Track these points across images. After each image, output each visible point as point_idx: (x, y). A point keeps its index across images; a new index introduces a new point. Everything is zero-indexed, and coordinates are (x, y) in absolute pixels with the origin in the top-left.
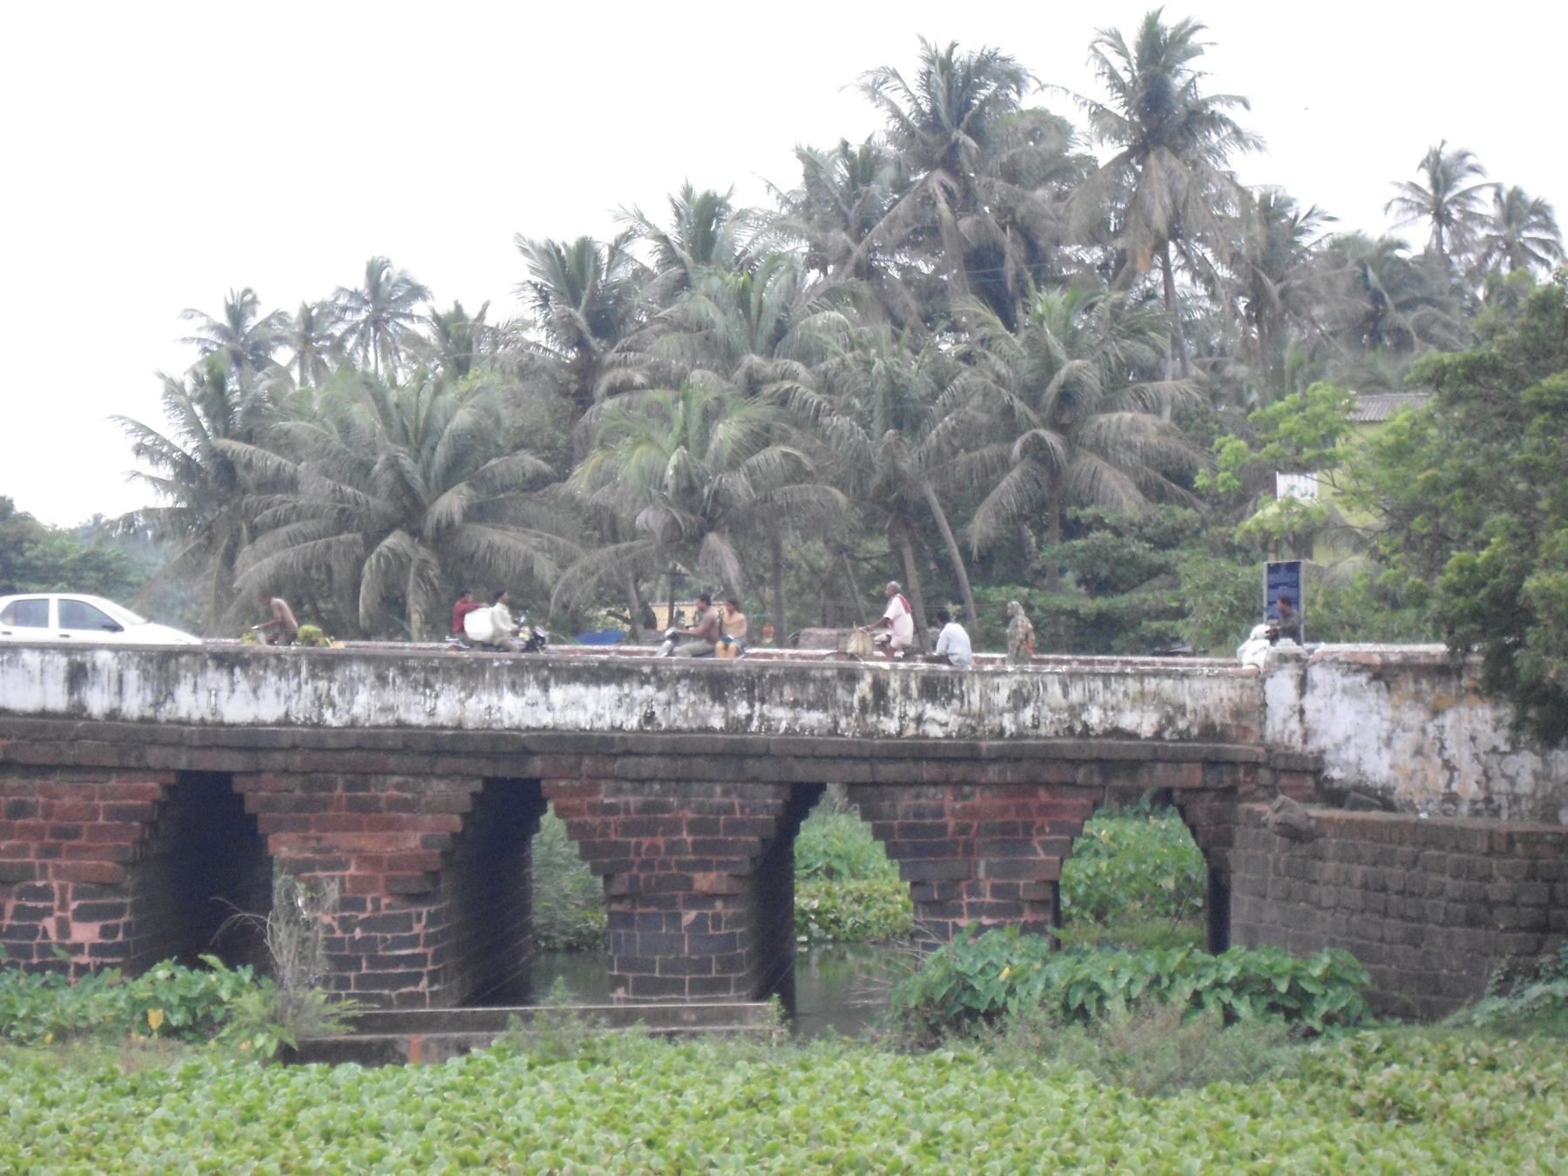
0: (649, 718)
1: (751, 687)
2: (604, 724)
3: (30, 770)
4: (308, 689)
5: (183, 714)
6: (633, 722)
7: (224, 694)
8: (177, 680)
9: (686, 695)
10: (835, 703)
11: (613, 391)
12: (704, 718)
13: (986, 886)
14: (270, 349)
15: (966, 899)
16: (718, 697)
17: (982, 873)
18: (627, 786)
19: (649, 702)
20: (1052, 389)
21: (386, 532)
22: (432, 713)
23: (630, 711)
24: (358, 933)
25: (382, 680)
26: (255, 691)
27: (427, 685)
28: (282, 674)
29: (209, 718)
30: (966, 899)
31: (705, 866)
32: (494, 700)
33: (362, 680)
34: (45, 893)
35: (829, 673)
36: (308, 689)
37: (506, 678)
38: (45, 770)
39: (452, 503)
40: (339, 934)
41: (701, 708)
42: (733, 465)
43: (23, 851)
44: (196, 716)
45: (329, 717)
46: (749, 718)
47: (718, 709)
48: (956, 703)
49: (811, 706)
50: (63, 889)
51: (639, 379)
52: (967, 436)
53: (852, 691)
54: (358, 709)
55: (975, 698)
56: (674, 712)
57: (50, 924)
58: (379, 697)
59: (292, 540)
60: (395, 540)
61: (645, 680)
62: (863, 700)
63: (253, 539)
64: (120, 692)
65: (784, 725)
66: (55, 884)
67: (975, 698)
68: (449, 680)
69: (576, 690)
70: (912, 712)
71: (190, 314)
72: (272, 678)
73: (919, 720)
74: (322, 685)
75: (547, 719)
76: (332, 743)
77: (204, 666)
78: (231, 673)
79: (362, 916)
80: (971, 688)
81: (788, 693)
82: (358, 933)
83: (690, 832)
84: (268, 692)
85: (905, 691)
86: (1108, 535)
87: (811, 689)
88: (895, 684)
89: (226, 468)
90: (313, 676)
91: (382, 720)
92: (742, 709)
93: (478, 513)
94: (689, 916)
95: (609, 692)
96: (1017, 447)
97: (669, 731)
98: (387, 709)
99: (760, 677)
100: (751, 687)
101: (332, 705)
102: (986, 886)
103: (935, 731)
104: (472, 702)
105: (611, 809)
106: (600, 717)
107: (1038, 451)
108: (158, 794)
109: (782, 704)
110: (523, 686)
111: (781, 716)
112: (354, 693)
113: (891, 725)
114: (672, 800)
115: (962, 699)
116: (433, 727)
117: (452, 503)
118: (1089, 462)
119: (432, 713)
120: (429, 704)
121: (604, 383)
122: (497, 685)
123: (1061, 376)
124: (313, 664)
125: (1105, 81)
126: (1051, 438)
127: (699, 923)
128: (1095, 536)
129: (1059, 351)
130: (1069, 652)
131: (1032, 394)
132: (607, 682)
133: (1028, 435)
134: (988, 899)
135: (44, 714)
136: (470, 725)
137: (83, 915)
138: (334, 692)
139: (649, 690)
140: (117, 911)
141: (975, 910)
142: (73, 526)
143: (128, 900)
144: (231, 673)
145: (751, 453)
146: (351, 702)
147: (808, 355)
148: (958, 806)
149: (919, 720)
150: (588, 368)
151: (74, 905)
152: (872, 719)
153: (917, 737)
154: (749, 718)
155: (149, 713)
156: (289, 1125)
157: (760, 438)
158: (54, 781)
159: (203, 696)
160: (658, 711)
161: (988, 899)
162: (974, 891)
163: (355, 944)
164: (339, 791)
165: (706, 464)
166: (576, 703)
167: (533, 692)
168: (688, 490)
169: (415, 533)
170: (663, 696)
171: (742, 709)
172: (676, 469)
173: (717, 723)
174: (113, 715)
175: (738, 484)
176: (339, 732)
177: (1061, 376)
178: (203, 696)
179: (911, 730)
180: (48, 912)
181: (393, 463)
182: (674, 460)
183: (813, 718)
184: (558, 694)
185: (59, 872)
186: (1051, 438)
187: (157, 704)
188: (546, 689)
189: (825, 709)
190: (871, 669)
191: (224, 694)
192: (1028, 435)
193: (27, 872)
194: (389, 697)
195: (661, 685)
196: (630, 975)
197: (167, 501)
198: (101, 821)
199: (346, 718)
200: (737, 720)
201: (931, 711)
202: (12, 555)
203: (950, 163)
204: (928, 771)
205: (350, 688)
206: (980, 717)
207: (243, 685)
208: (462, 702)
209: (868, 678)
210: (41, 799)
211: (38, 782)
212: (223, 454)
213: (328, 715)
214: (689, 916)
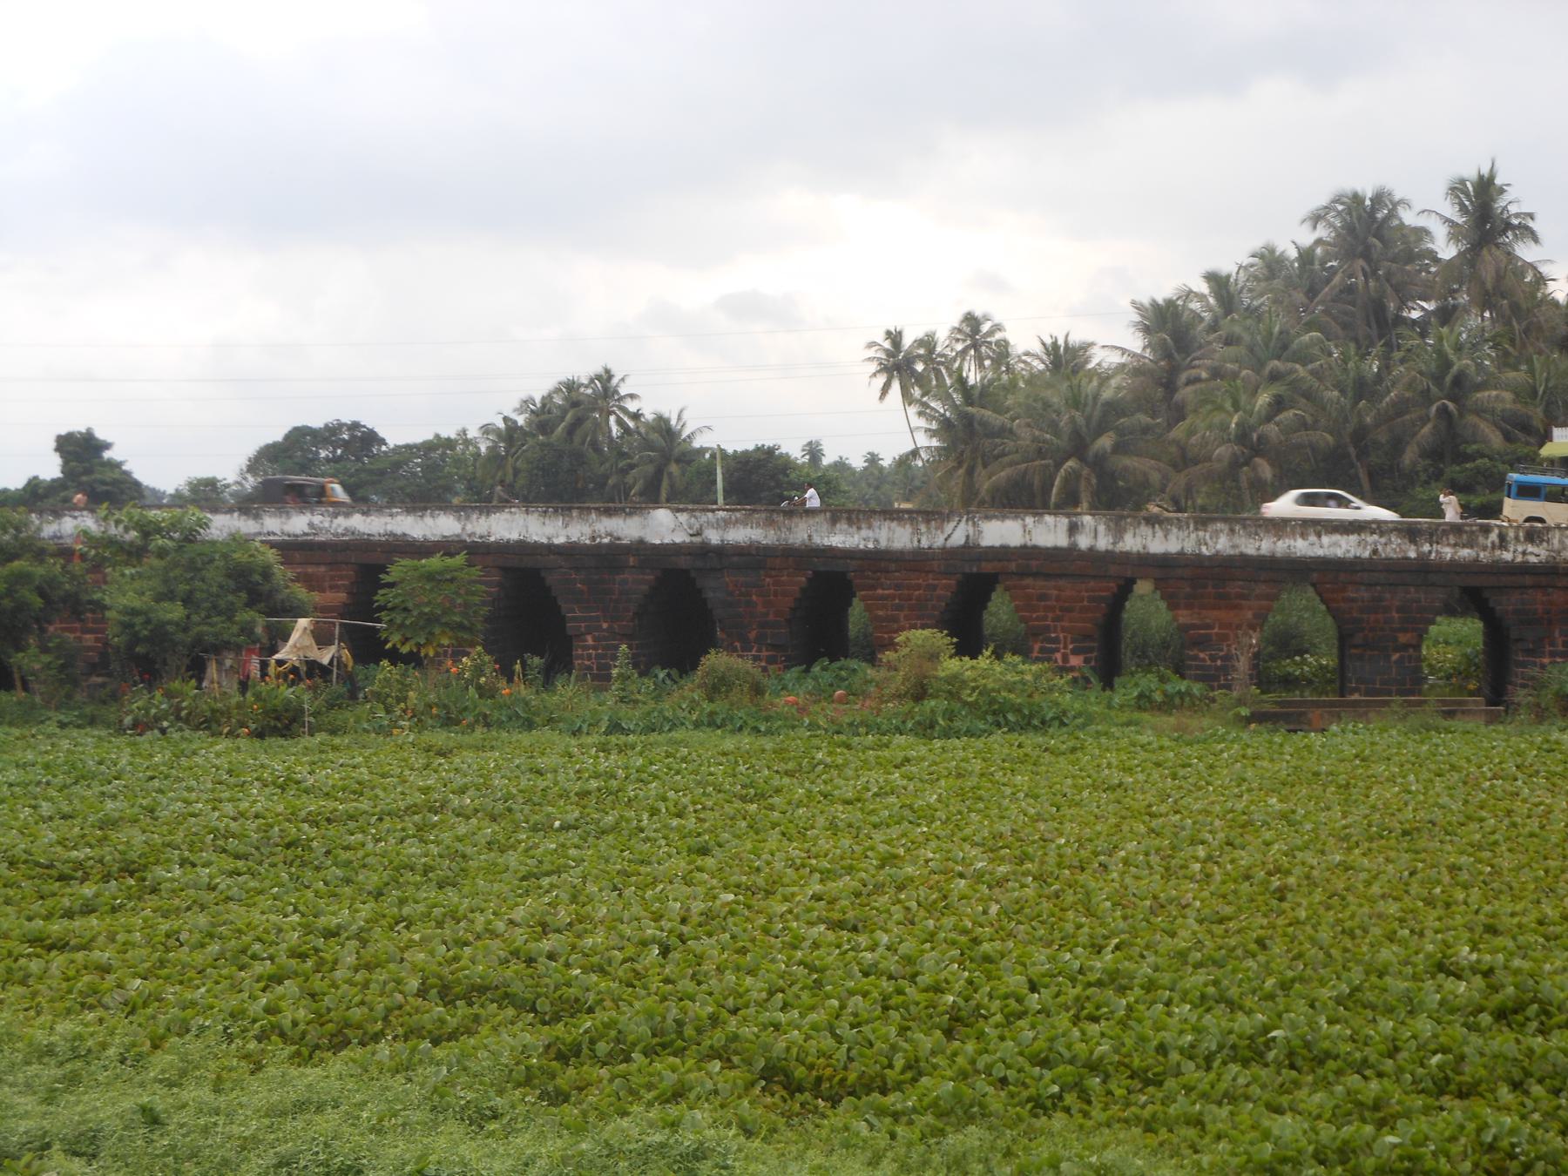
0: (1375, 552)
1: (1431, 535)
2: (1351, 555)
3: (1048, 576)
4: (1193, 536)
5: (1127, 548)
6: (1366, 554)
7: (1150, 538)
8: (1125, 530)
9: (1396, 540)
10: (1478, 545)
11: (1189, 382)
12: (1405, 552)
13: (1560, 641)
14: (913, 363)
15: (1548, 648)
16: (1413, 541)
17: (1557, 634)
18: (1363, 588)
19: (1375, 543)
20: (1448, 379)
21: (1067, 459)
22: (1259, 549)
23: (1365, 548)
24: (1219, 663)
25: (1232, 531)
26: (1166, 537)
27: (1257, 534)
28: (1180, 528)
29: (1141, 550)
30: (1548, 648)
31: (1405, 631)
32: (1292, 542)
33: (1222, 531)
34: (1056, 640)
35: (1474, 528)
36: (1193, 536)
37: (1298, 530)
38: (1060, 576)
39: (1106, 442)
40: (1209, 663)
41: (1403, 547)
42: (1269, 419)
43: (1045, 618)
44: (1135, 550)
45: (1204, 549)
46: (1430, 552)
47: (1413, 547)
48: (1545, 544)
49: (1464, 546)
50: (1065, 638)
51: (1204, 375)
52: (1401, 407)
53: (1487, 538)
54: (1219, 547)
55: (1556, 541)
56: (1388, 549)
57: (1058, 656)
58: (1231, 540)
59: (1011, 464)
60: (1070, 463)
61: (1373, 533)
62: (1493, 543)
63: (985, 466)
64: (1096, 537)
65: (1449, 556)
66: (1061, 635)
67: (1556, 541)
68: (1268, 531)
69: (1337, 537)
70: (1520, 549)
71: (871, 345)
72: (1175, 530)
73: (1524, 553)
74: (1201, 534)
75: (1320, 552)
76: (1207, 564)
77: (1139, 523)
78: (1153, 527)
79: (1221, 654)
80: (1554, 537)
81: (1452, 540)
82: (1219, 663)
83: (1397, 612)
84: (1172, 537)
85: (1517, 538)
86: (1486, 460)
87: (1465, 537)
88: (1511, 534)
89: (968, 421)
90: (1196, 529)
91: (1232, 553)
92: (1426, 548)
93: (1119, 448)
94: (1395, 657)
95: (1353, 538)
96: (1434, 409)
97: (1386, 559)
98: (1234, 547)
99: (1436, 530)
100: (1431, 535)
101: (1206, 544)
102: (1560, 641)
103: (1533, 559)
104: (1280, 543)
105: (1353, 600)
106: (1348, 551)
107: (1443, 411)
108: (1115, 590)
109: (1449, 545)
110: (1308, 535)
111: (1447, 552)
112: (1217, 538)
113: (1507, 556)
114: (1388, 596)
115: (1548, 542)
116: (1259, 556)
117: (1106, 442)
118: (1472, 419)
119: (1259, 549)
120: (1257, 544)
121: (1183, 377)
122: (1293, 534)
123: (1455, 368)
124: (1196, 523)
125: (1457, 208)
126: (1451, 406)
127: (1401, 661)
128: (1479, 461)
129: (1452, 357)
130: (722, 551)
131: (1438, 379)
132: (1352, 533)
133: (1439, 403)
134: (1561, 648)
135: (1056, 549)
136: (1278, 555)
137: (1075, 652)
138: (1207, 537)
139: (1376, 537)
140: (1091, 650)
141: (1553, 654)
142: (138, 475)
143: (1096, 645)
144: (1153, 527)
145: (1276, 415)
146: (1216, 543)
147: (1304, 359)
148: (1545, 598)
149: (1524, 553)
150: (1174, 371)
151: (1071, 647)
152: (1498, 552)
153: (1523, 562)
154: (1430, 552)
155: (1110, 547)
156: (1244, 756)
157: (1278, 404)
158: (1061, 582)
159: (1139, 539)
160: (1380, 548)
161: (1561, 648)
162: (1552, 644)
163: (1217, 669)
164: (1210, 589)
165: (1252, 421)
166: (1336, 544)
167: (1313, 538)
168: (1243, 436)
169: (1082, 459)
170: (1383, 540)
171: (1426, 548)
172: (1237, 424)
173: (1412, 555)
174: (1091, 549)
175: (1272, 430)
176: (1210, 558)
177: (1455, 368)
178: (1139, 539)
179: (1519, 559)
180: (1057, 650)
181: (1072, 419)
182: (1235, 419)
183: (1465, 553)
184: (1326, 540)
185: (1063, 630)
186: (1451, 406)
187: (1114, 544)
188: (1319, 536)
189: (1472, 547)
190: (1498, 526)
191: (1150, 538)
192: (1439, 403)
193: (1047, 629)
194: (1237, 540)
195: (1382, 534)
196: (1362, 686)
197: (935, 443)
198: (1085, 603)
199: (1213, 551)
200: (1424, 553)
201: (1530, 548)
202: (781, 477)
203: (1366, 256)
204: (1528, 580)
205: (1216, 533)
206: (1559, 552)
207: (1160, 534)
208: (1275, 543)
209: (1496, 531)
210: (1056, 592)
211: (1053, 583)
212: (967, 414)
213: (1204, 549)
214: (1395, 657)
